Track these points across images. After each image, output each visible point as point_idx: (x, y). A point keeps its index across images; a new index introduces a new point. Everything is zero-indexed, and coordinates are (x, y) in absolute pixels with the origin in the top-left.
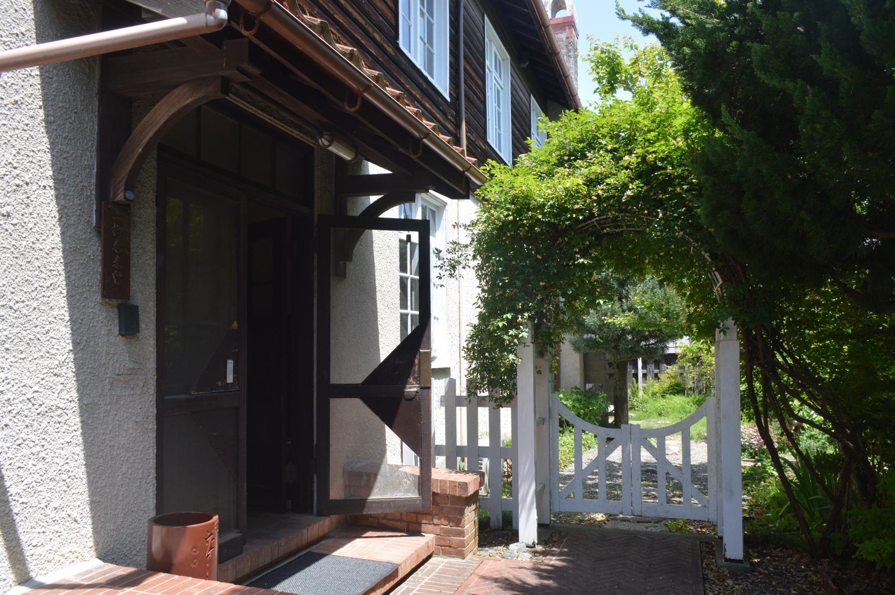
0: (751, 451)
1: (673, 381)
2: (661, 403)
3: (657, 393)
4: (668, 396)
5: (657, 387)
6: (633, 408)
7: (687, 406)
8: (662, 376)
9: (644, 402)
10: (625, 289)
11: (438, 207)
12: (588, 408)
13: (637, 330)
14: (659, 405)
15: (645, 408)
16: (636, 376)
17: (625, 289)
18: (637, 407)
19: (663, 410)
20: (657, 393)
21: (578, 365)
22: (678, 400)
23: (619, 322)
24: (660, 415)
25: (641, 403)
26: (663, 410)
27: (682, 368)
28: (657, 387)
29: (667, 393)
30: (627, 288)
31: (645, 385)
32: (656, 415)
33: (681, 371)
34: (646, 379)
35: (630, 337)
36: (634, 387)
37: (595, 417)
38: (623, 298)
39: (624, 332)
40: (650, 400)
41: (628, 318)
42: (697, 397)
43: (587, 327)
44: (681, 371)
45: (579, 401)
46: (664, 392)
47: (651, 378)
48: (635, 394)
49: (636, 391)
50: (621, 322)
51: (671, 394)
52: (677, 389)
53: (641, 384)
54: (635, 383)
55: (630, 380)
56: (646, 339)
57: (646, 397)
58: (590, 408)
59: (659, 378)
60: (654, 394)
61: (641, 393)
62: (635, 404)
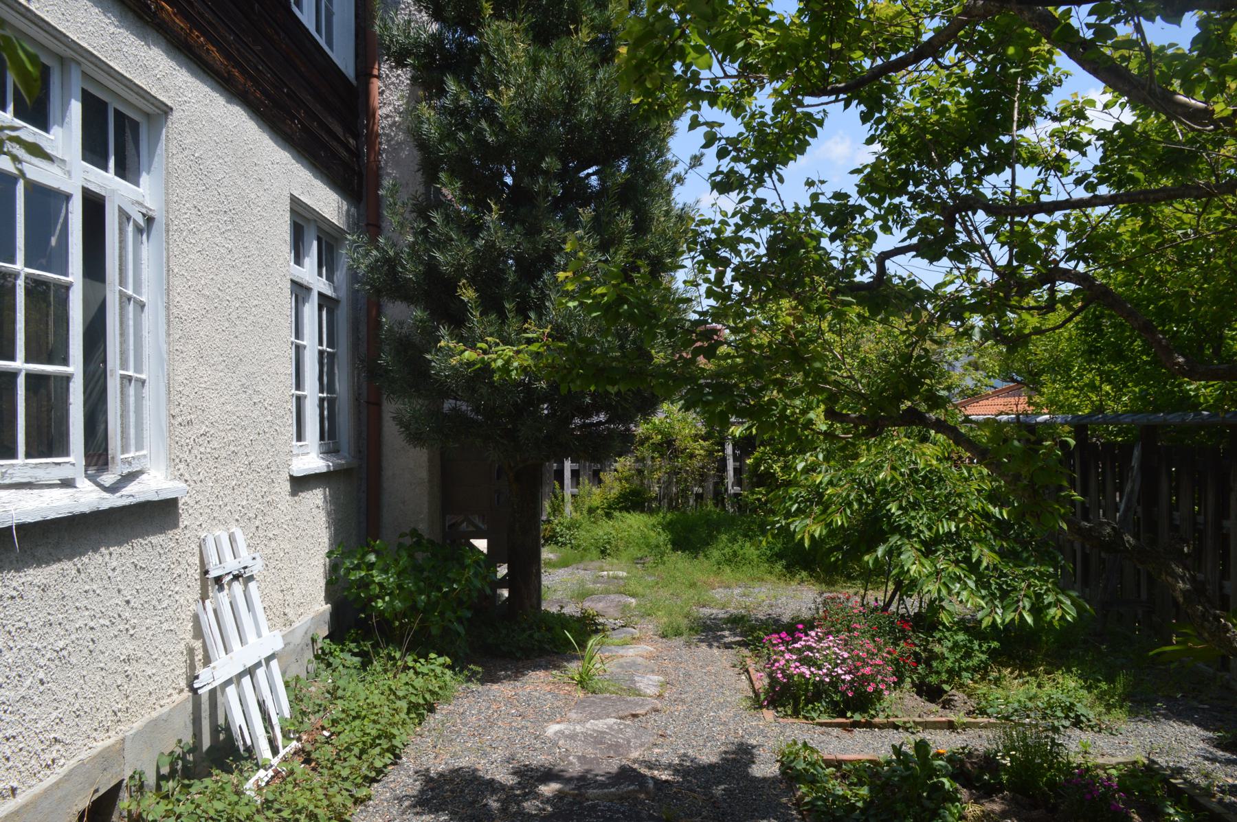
0: (837, 698)
1: (627, 486)
2: (604, 529)
3: (598, 508)
4: (617, 514)
5: (596, 496)
6: (552, 539)
7: (652, 534)
8: (607, 477)
9: (573, 525)
10: (536, 288)
11: (148, 115)
12: (439, 589)
13: (564, 390)
14: (601, 533)
15: (575, 538)
16: (559, 475)
17: (536, 288)
18: (561, 536)
19: (609, 543)
20: (598, 508)
21: (424, 474)
22: (635, 522)
23: (500, 363)
24: (603, 552)
25: (569, 529)
26: (609, 543)
27: (640, 460)
28: (596, 496)
29: (615, 509)
30: (540, 284)
31: (575, 491)
32: (595, 553)
33: (639, 466)
34: (578, 484)
35: (545, 409)
36: (556, 497)
37: (455, 612)
38: (530, 309)
39: (531, 397)
40: (586, 524)
41: (534, 348)
42: (669, 516)
43: (436, 381)
44: (639, 466)
45: (417, 569)
46: (610, 507)
47: (587, 481)
48: (556, 510)
49: (559, 506)
50: (508, 362)
51: (621, 510)
52: (633, 501)
53: (569, 490)
54: (558, 491)
55: (551, 484)
56: (586, 412)
57: (577, 516)
58: (445, 590)
59: (600, 481)
60: (591, 511)
61: (568, 508)
62: (558, 530)
